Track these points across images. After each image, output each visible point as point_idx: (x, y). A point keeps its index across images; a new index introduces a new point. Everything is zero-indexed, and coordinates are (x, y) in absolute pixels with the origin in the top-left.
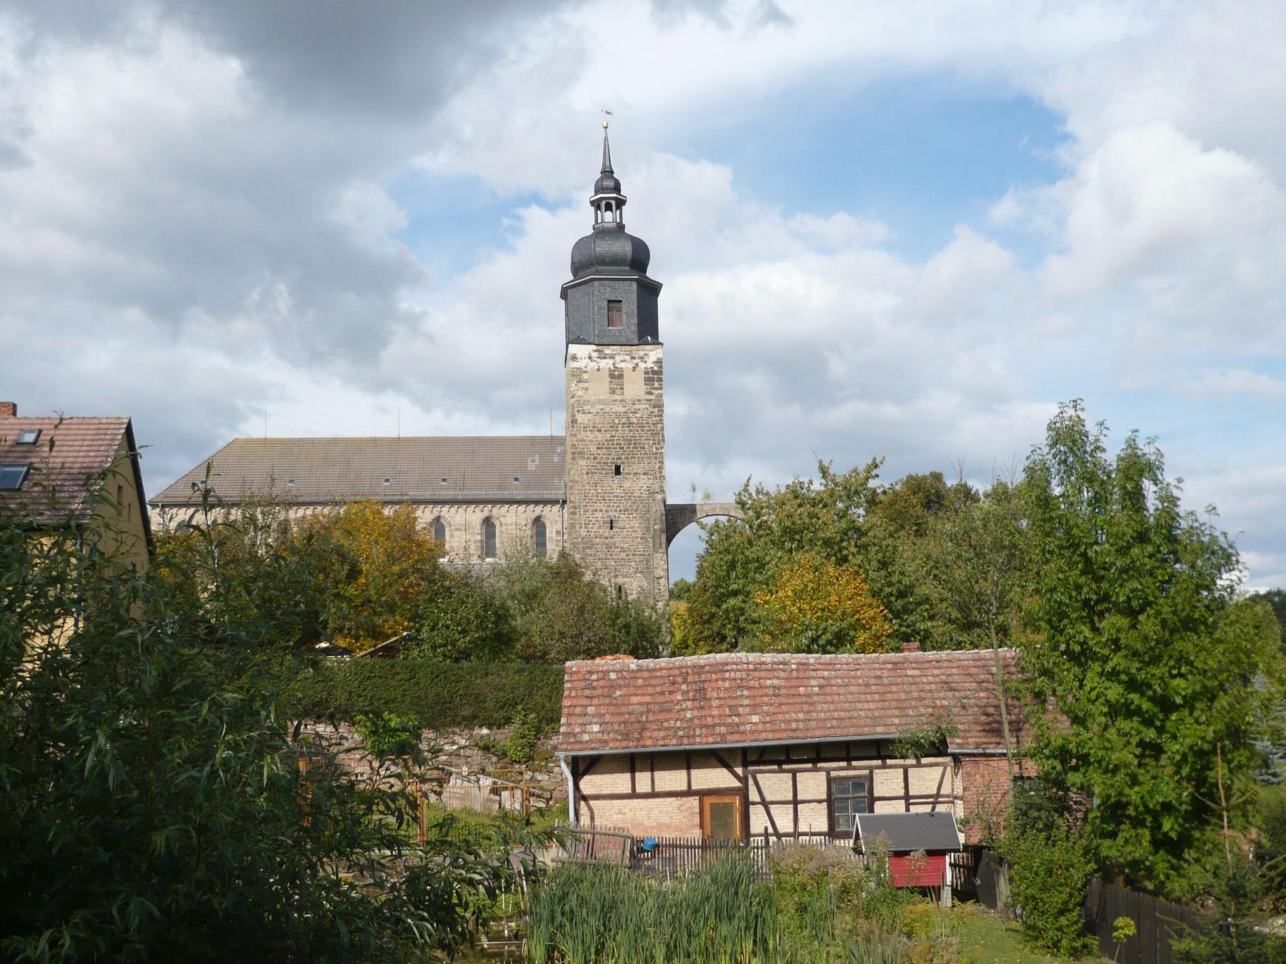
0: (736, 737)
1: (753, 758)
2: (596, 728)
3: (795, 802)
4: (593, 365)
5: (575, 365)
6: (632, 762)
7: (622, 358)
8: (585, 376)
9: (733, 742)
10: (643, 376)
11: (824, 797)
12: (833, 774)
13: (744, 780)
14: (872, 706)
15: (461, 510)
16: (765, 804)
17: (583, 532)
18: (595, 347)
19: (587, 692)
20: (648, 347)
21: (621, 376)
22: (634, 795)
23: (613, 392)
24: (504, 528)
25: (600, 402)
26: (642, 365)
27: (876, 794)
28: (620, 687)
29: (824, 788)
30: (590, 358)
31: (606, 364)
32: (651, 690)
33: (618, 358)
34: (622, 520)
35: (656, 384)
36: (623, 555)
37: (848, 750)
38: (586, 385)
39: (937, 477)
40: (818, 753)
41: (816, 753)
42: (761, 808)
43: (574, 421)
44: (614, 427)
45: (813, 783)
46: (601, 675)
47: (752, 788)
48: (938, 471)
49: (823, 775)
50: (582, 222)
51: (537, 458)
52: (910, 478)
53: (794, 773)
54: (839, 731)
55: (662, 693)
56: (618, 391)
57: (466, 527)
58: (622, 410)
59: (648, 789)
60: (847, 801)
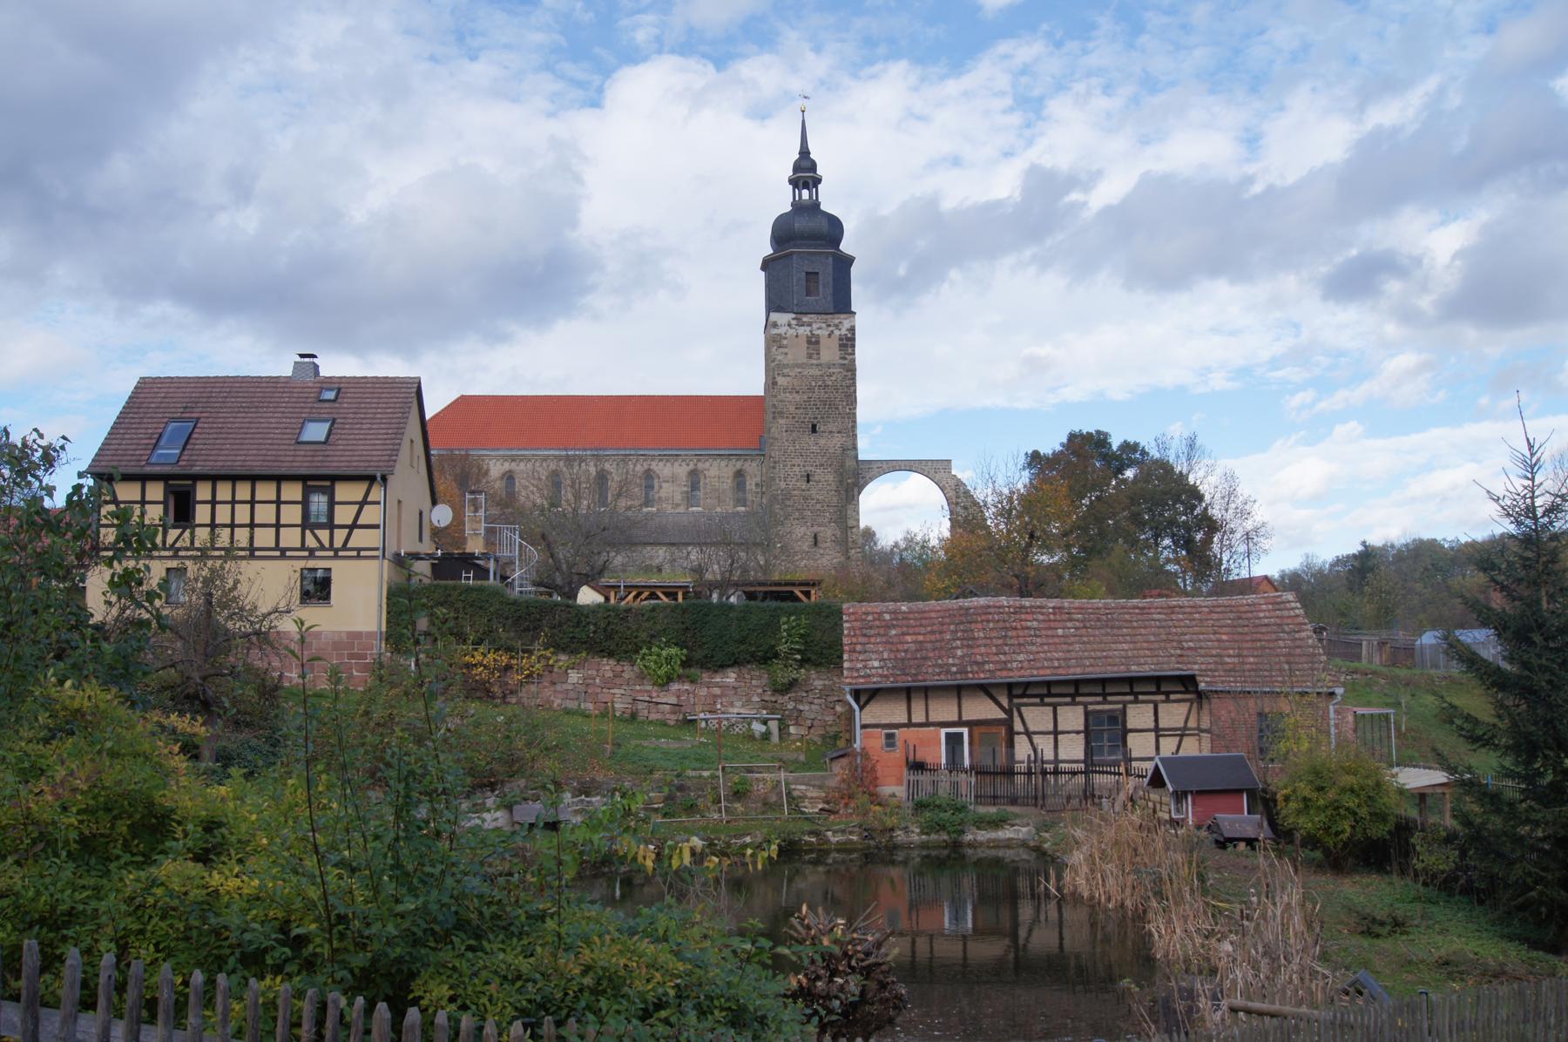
0: (1004, 673)
1: (1020, 691)
2: (876, 664)
3: (1056, 733)
4: (792, 332)
5: (775, 331)
6: (908, 693)
7: (819, 327)
9: (1002, 677)
11: (1082, 728)
12: (1090, 707)
13: (1009, 712)
14: (1126, 646)
15: (715, 463)
16: (1029, 734)
17: (783, 485)
21: (817, 342)
22: (910, 724)
23: (810, 356)
25: (798, 366)
26: (837, 333)
27: (1129, 726)
28: (894, 627)
29: (1081, 720)
31: (804, 331)
32: (922, 630)
34: (819, 474)
37: (1103, 685)
40: (1077, 689)
41: (1075, 688)
42: (1024, 737)
43: (775, 383)
44: (811, 389)
45: (1072, 717)
47: (1017, 720)
48: (1088, 427)
49: (1080, 709)
50: (782, 200)
53: (1055, 706)
54: (1097, 669)
55: (932, 632)
57: (673, 479)
59: (922, 719)
60: (1106, 734)
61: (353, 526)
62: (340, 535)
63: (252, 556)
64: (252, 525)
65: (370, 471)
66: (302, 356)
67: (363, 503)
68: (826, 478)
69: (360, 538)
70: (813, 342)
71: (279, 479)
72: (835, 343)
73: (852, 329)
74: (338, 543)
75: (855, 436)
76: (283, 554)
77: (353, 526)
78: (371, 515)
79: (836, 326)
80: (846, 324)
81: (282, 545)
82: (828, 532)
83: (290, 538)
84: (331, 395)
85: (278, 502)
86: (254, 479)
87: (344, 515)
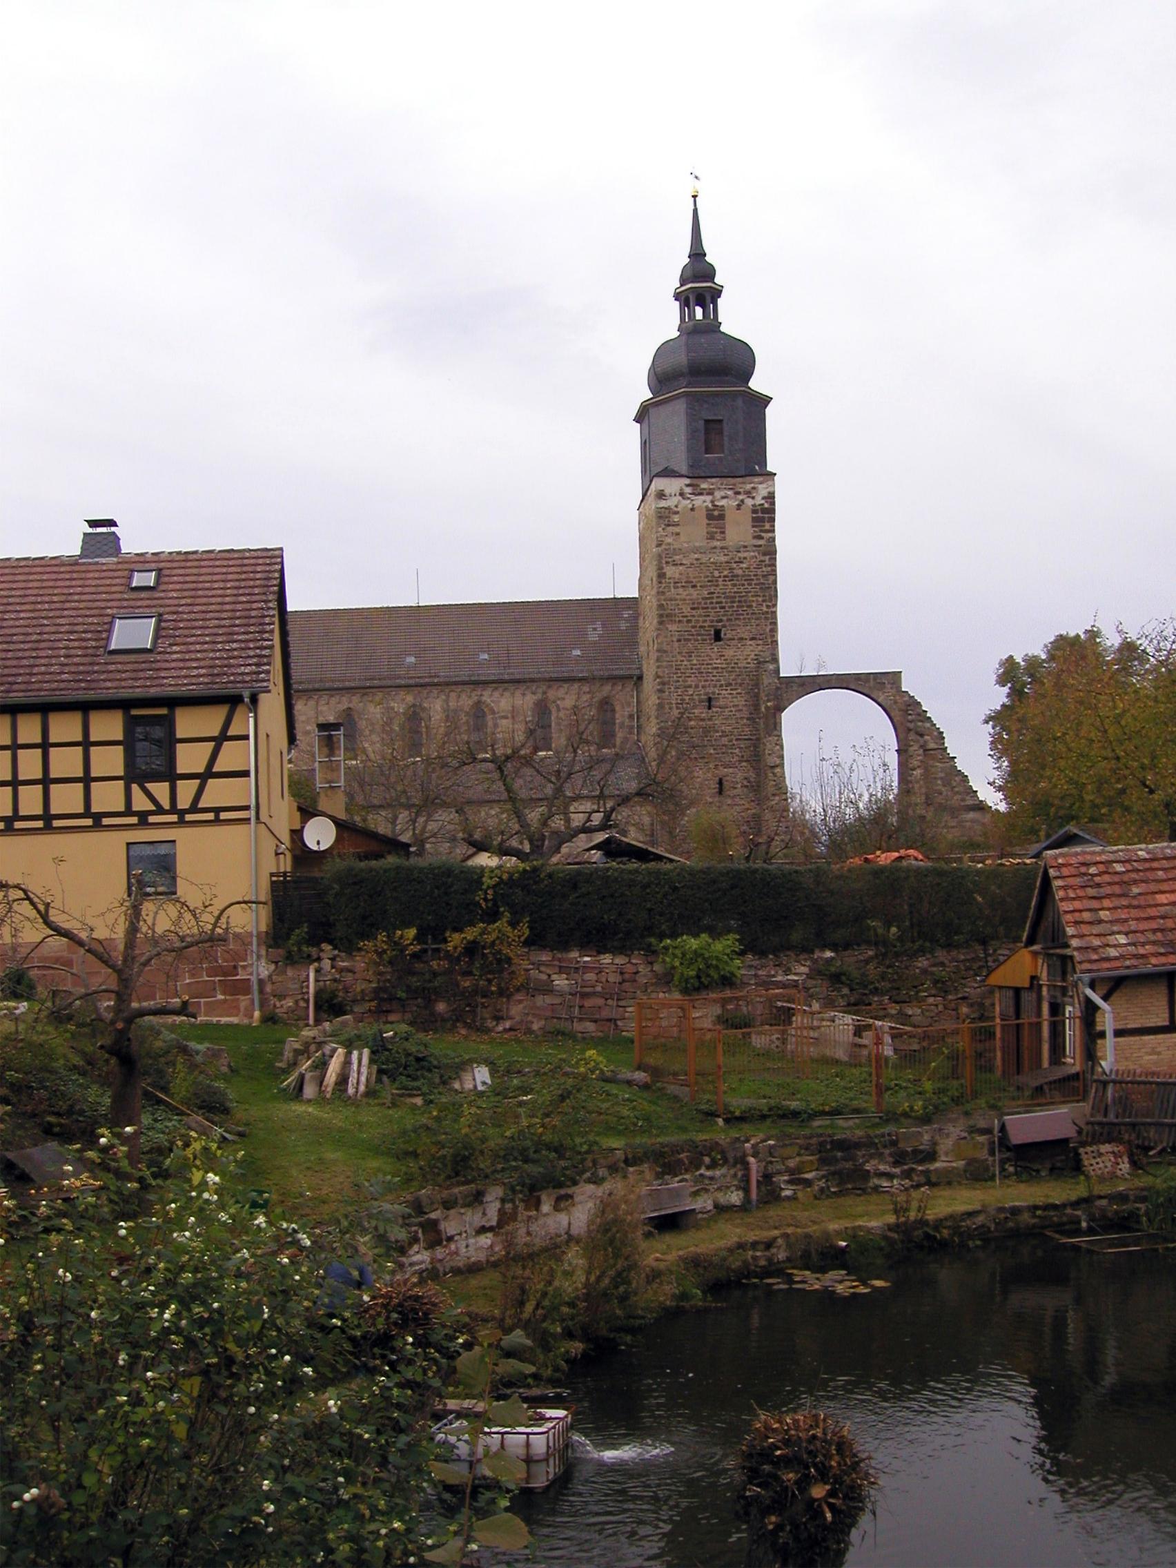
2: (1122, 940)
5: (663, 504)
8: (676, 518)
10: (749, 516)
18: (688, 481)
19: (1091, 892)
20: (756, 479)
23: (711, 537)
24: (561, 714)
25: (696, 550)
30: (682, 494)
33: (718, 494)
35: (767, 526)
36: (725, 740)
38: (676, 529)
39: (1093, 634)
44: (713, 581)
46: (1102, 868)
51: (598, 625)
52: (1061, 638)
56: (718, 536)
58: (723, 559)
61: (209, 774)
62: (186, 791)
63: (48, 828)
64: (46, 781)
65: (231, 690)
66: (93, 523)
67: (222, 738)
68: (733, 701)
69: (218, 793)
70: (716, 517)
71: (85, 708)
72: (746, 517)
73: (771, 497)
74: (184, 802)
75: (775, 643)
76: (98, 821)
77: (209, 774)
78: (229, 758)
79: (748, 493)
80: (763, 491)
81: (94, 810)
82: (738, 775)
83: (108, 797)
84: (149, 579)
85: (86, 744)
86: (45, 709)
87: (190, 759)
